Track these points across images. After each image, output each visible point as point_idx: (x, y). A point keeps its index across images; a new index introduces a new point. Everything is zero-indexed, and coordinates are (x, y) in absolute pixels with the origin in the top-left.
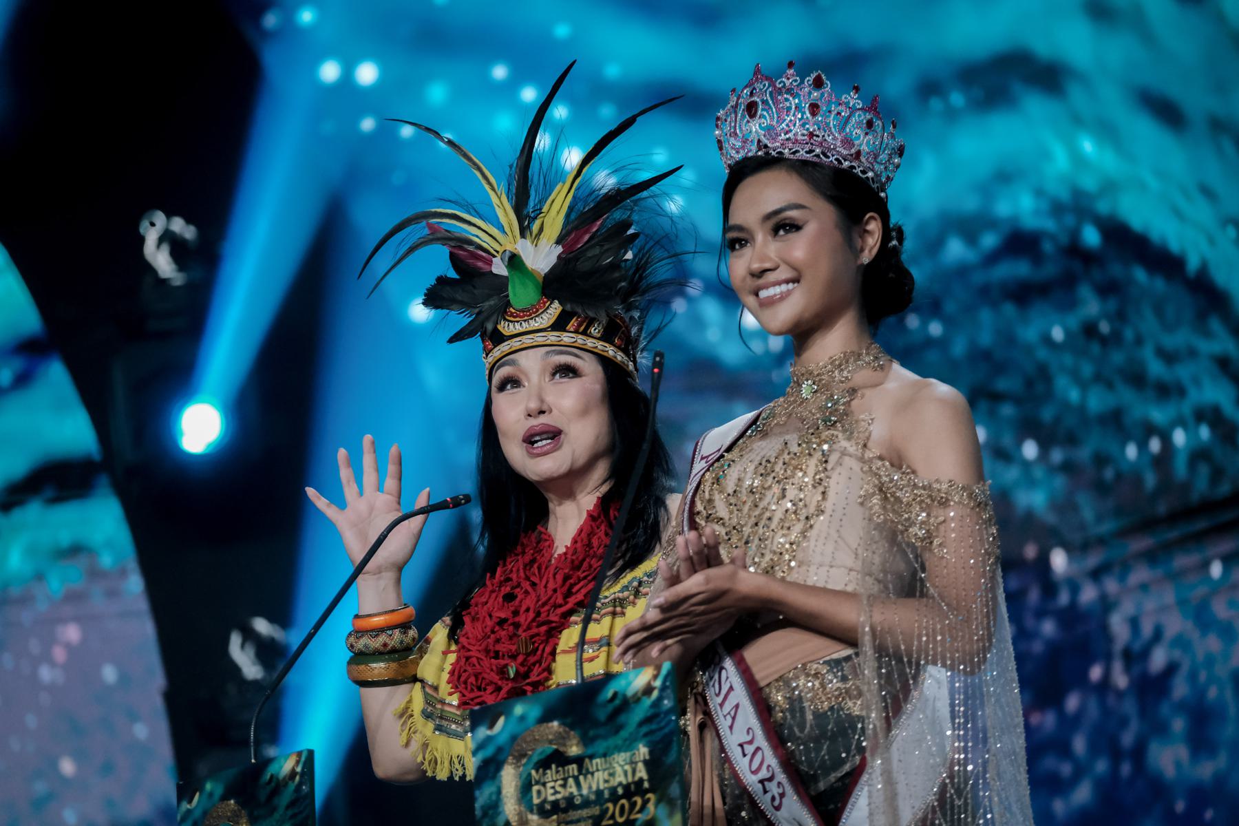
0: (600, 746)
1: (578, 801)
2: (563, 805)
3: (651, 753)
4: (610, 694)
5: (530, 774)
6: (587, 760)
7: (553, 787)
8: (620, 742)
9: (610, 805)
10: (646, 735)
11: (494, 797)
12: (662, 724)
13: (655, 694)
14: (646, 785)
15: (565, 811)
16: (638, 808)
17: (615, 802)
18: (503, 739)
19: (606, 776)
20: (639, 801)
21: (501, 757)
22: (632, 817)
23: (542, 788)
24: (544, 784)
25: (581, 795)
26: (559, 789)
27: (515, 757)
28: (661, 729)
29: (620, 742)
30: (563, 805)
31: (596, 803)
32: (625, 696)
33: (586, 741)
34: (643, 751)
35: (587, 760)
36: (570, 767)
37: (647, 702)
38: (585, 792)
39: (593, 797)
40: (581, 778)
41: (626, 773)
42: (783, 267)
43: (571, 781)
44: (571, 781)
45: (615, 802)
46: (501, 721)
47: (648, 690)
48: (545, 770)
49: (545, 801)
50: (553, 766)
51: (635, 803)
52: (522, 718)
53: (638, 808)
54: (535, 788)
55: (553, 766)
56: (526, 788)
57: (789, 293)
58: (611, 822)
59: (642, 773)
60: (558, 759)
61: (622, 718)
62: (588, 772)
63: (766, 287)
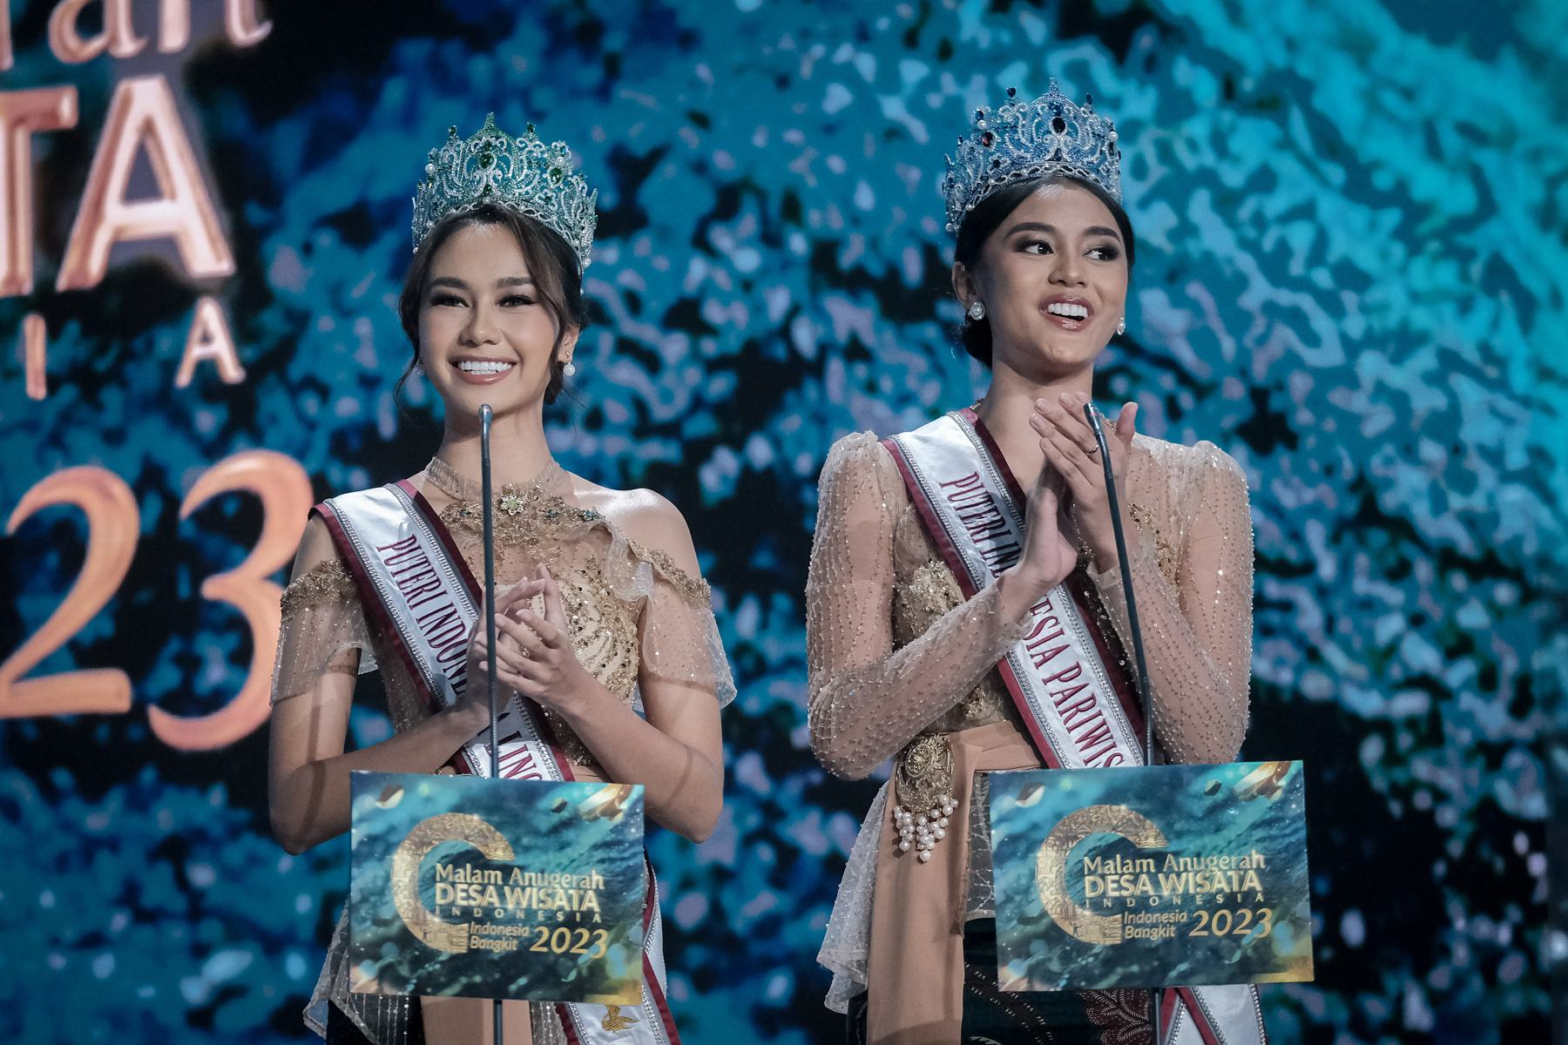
0: (1192, 845)
1: (499, 914)
2: (478, 914)
3: (606, 883)
4: (556, 803)
5: (434, 867)
6: (516, 870)
7: (1118, 882)
8: (1222, 843)
9: (1205, 916)
10: (602, 861)
11: (380, 883)
12: (626, 855)
13: (619, 818)
14: (597, 918)
15: (1135, 911)
16: (582, 942)
17: (552, 928)
18: (400, 818)
19: (1199, 879)
20: (1249, 915)
21: (393, 838)
22: (573, 950)
23: (450, 888)
24: (453, 884)
25: (1160, 897)
26: (473, 895)
27: (415, 843)
28: (623, 859)
29: (1222, 843)
30: (478, 914)
31: (525, 923)
32: (576, 810)
33: (1169, 832)
34: (597, 878)
35: (516, 870)
36: (493, 873)
37: (607, 825)
38: (1166, 893)
39: (522, 915)
40: (507, 889)
41: (570, 899)
42: (503, 344)
43: (491, 889)
44: (491, 889)
45: (552, 928)
46: (398, 797)
47: (610, 811)
48: (455, 867)
49: (452, 904)
50: (468, 866)
51: (581, 935)
52: (428, 800)
53: (582, 942)
54: (440, 886)
55: (468, 866)
56: (427, 882)
57: (505, 373)
58: (545, 950)
59: (592, 903)
60: (477, 860)
61: (569, 835)
62: (516, 884)
63: (472, 359)
